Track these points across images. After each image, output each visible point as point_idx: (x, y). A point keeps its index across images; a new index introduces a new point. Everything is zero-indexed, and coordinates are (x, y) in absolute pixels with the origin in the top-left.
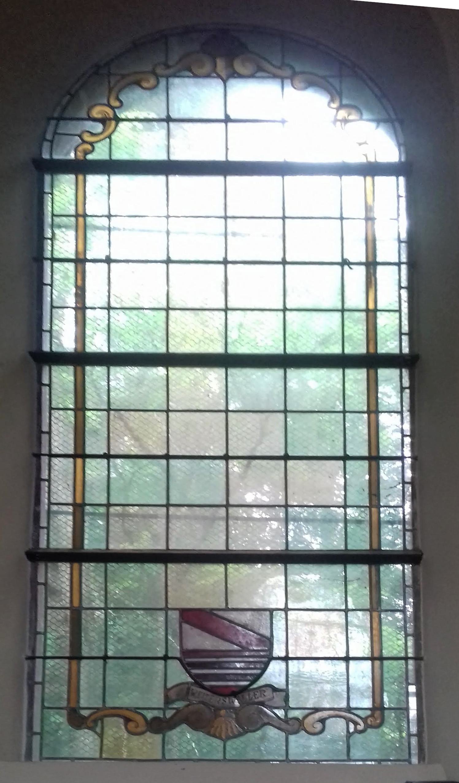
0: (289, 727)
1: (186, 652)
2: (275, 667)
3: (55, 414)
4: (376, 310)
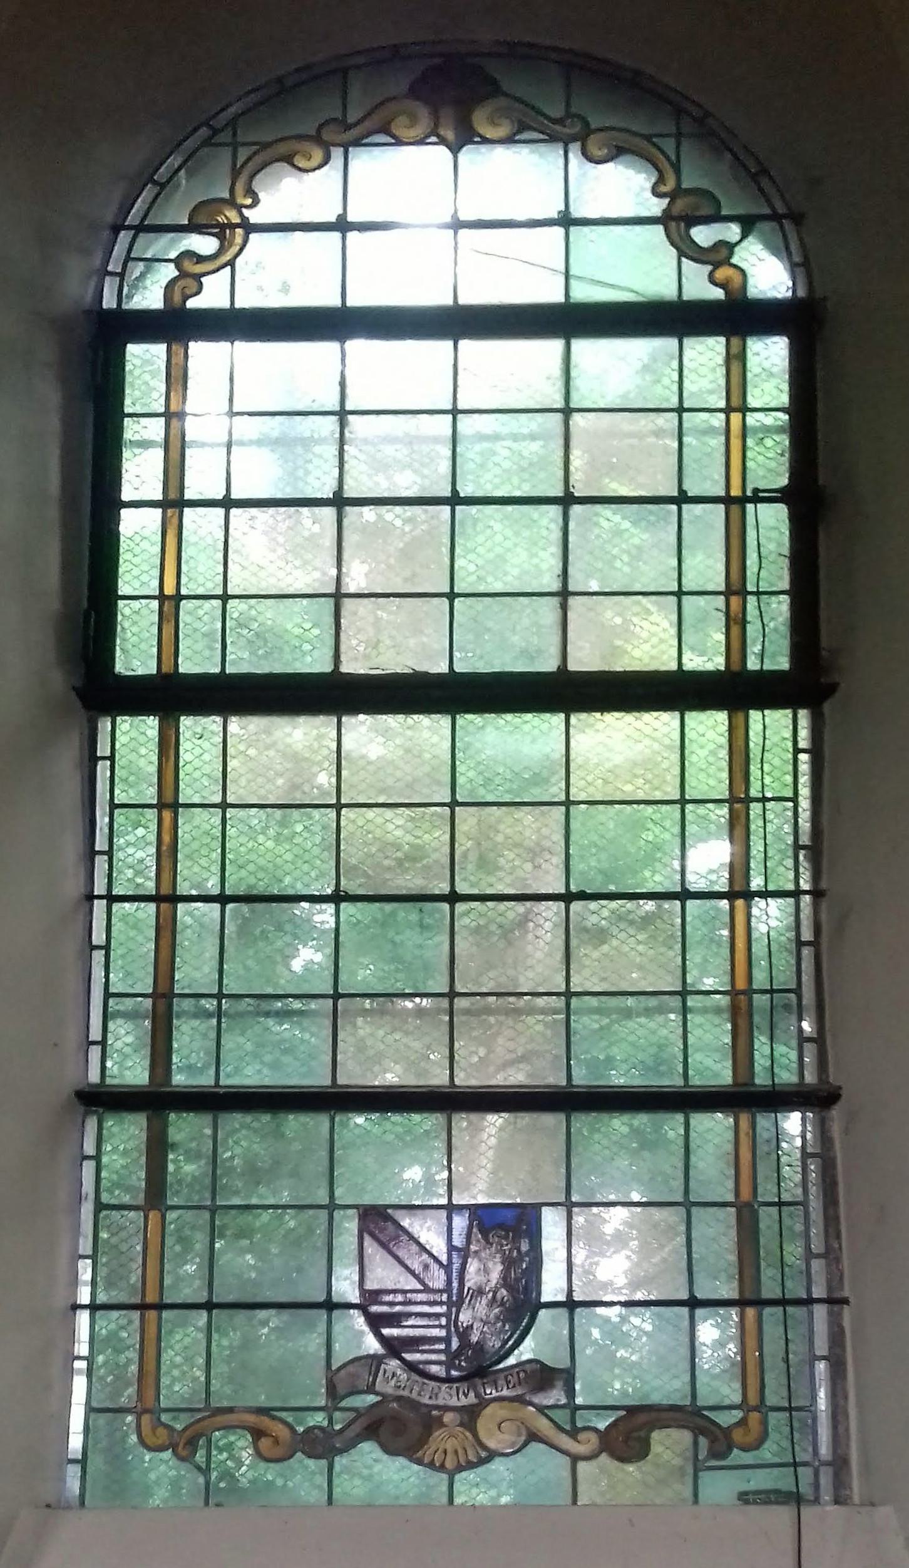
0: (576, 1444)
1: (371, 1296)
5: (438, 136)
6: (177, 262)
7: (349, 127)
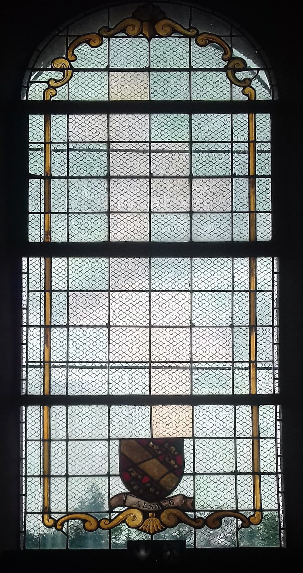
3: (29, 443)
4: (256, 291)
5: (143, 34)
7: (110, 30)
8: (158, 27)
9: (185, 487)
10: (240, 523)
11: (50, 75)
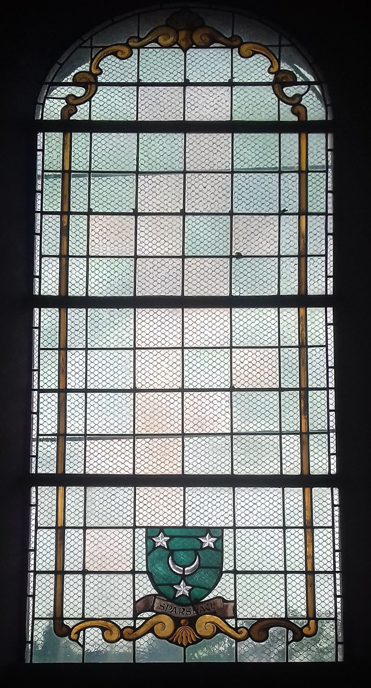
2: (227, 580)
6: (66, 99)
7: (140, 40)
8: (196, 38)
9: (224, 589)
10: (291, 634)
11: (70, 90)
